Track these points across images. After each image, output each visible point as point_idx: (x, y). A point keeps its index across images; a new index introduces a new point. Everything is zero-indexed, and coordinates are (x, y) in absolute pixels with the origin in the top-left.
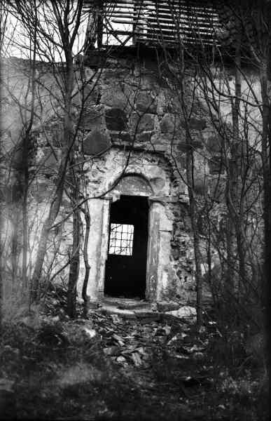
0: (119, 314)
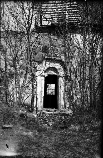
0: (48, 113)
